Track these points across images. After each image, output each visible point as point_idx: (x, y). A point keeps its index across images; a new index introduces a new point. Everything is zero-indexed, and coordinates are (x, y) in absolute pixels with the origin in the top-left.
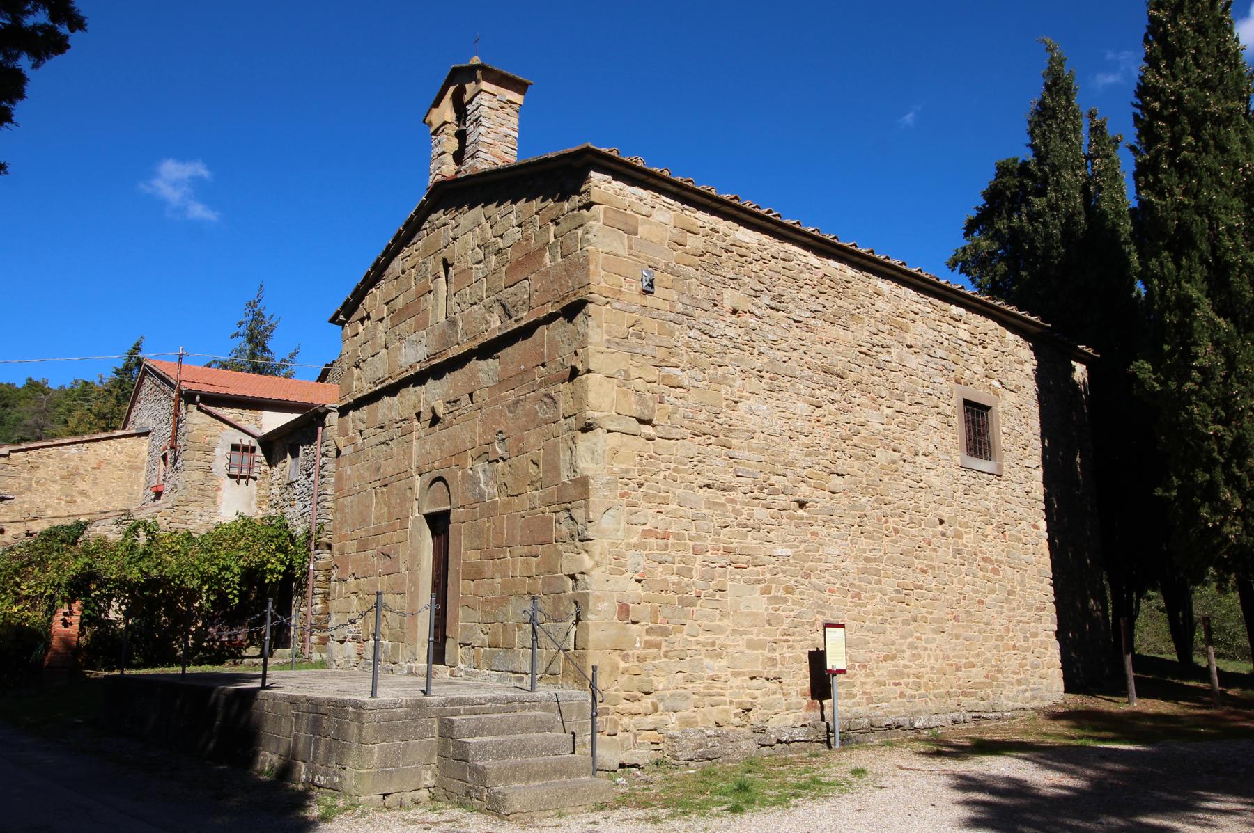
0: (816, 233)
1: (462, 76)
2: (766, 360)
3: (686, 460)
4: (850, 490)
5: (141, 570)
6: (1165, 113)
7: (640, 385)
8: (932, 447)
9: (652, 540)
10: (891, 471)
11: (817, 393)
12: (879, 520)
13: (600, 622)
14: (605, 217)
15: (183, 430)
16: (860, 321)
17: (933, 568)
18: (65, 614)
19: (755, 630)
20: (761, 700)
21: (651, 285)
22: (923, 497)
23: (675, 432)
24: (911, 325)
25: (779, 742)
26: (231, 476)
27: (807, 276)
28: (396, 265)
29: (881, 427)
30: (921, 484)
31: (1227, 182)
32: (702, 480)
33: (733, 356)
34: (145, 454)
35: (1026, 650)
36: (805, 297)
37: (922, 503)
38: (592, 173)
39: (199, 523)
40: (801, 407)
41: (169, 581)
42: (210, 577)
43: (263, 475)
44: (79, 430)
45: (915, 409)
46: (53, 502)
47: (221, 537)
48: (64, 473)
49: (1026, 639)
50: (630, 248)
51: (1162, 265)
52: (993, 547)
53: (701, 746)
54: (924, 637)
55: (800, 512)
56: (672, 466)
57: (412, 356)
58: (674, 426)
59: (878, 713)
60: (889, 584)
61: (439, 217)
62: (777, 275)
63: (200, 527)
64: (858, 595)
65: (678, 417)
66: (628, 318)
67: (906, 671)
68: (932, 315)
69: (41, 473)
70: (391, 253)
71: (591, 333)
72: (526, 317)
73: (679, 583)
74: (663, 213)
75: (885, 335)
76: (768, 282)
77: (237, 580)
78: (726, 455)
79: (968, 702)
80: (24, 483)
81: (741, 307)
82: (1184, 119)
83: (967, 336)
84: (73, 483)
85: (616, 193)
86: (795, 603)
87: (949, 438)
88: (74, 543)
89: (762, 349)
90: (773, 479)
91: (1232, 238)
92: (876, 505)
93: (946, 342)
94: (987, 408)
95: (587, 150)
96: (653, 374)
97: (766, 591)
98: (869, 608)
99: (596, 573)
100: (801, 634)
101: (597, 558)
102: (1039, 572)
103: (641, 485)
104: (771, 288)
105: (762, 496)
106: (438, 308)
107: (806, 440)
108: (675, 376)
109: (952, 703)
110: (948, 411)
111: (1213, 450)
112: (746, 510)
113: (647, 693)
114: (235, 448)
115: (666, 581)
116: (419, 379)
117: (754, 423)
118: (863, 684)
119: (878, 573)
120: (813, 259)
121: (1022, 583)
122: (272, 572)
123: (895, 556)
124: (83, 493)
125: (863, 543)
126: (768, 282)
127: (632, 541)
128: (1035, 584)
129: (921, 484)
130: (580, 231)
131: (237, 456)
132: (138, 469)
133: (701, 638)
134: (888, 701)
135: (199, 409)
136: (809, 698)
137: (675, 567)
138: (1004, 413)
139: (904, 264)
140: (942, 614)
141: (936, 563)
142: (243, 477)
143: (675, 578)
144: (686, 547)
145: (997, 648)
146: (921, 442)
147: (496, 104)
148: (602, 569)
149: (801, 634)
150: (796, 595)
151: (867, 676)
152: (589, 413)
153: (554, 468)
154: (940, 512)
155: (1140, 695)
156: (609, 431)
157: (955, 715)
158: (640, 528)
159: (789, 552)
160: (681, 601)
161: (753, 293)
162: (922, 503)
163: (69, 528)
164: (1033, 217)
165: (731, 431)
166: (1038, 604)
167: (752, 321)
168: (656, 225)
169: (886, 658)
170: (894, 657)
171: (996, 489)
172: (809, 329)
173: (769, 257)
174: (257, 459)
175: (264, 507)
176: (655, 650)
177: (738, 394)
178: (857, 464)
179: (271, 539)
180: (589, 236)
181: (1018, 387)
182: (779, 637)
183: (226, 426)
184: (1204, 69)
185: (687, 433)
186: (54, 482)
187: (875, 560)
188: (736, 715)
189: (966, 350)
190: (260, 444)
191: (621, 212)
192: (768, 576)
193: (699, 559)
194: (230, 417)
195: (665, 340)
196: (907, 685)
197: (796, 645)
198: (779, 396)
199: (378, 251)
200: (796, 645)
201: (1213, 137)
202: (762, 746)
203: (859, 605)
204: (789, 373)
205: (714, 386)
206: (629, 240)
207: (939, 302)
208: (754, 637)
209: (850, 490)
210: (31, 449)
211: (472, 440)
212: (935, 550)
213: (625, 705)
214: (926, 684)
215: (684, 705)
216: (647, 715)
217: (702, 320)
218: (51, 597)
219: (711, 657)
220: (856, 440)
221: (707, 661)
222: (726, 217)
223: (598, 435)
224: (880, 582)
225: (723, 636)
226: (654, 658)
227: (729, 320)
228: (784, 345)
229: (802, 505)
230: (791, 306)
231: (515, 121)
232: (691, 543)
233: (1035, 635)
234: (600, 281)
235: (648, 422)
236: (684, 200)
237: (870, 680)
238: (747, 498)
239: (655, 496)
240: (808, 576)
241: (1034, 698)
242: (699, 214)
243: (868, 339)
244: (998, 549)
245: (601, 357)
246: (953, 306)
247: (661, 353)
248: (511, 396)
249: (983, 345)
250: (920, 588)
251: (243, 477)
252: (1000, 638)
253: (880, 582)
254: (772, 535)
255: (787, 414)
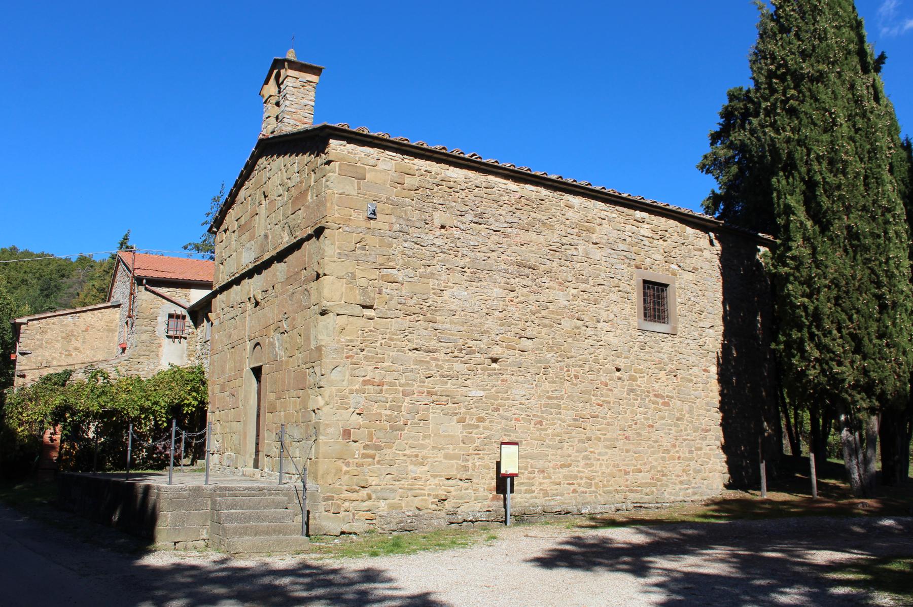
0: (512, 168)
1: (278, 64)
2: (468, 260)
3: (398, 332)
4: (537, 349)
5: (99, 404)
6: (779, 73)
7: (363, 282)
8: (612, 316)
9: (370, 387)
10: (574, 334)
11: (512, 281)
12: (562, 369)
13: (329, 440)
14: (340, 169)
15: (136, 304)
16: (551, 227)
17: (608, 402)
18: (51, 434)
19: (451, 447)
20: (453, 493)
21: (374, 213)
22: (602, 353)
23: (389, 314)
24: (598, 228)
25: (465, 521)
26: (169, 337)
27: (506, 198)
28: (242, 193)
29: (567, 303)
30: (601, 343)
31: (818, 122)
32: (411, 345)
33: (440, 258)
34: (118, 320)
35: (691, 460)
36: (504, 213)
37: (601, 357)
38: (331, 141)
39: (146, 371)
40: (497, 292)
41: (120, 412)
42: (147, 409)
43: (191, 336)
44: (87, 301)
45: (600, 289)
46: (57, 355)
47: (158, 382)
48: (64, 335)
49: (690, 452)
50: (359, 189)
51: (778, 181)
52: (665, 385)
53: (401, 522)
54: (597, 451)
55: (494, 365)
56: (387, 336)
57: (247, 260)
58: (389, 309)
59: (552, 503)
60: (568, 415)
61: (263, 161)
62: (480, 199)
63: (148, 373)
64: (541, 423)
65: (393, 303)
66: (355, 237)
67: (579, 475)
68: (618, 219)
69: (49, 336)
70: (239, 185)
71: (326, 249)
72: (300, 235)
73: (391, 415)
74: (387, 162)
75: (574, 237)
76: (472, 204)
77: (163, 411)
78: (432, 327)
79: (632, 496)
80: (38, 343)
81: (448, 224)
82: (789, 78)
83: (649, 233)
84: (70, 342)
85: (348, 152)
86: (485, 428)
87: (628, 309)
88: (64, 385)
89: (465, 253)
90: (470, 343)
91: (820, 164)
92: (559, 359)
93: (629, 239)
94: (666, 286)
95: (325, 127)
96: (375, 274)
97: (461, 421)
98: (549, 431)
99: (326, 409)
100: (489, 449)
101: (327, 399)
102: (707, 404)
103: (362, 350)
104: (475, 208)
105: (461, 355)
106: (261, 225)
107: (500, 315)
108: (392, 275)
109: (619, 497)
110: (629, 289)
111: (802, 316)
112: (446, 365)
113: (363, 487)
114: (171, 316)
115: (380, 414)
116: (249, 274)
117: (456, 305)
118: (541, 484)
119: (559, 407)
120: (511, 185)
121: (690, 411)
122: (189, 405)
123: (574, 394)
124: (76, 349)
125: (547, 385)
126: (472, 204)
127: (354, 388)
128: (702, 412)
129: (601, 343)
130: (324, 180)
131: (173, 322)
132: (112, 331)
133: (407, 452)
134: (562, 495)
135: (146, 289)
136: (495, 493)
137: (387, 405)
138: (681, 288)
139: (589, 184)
140: (615, 435)
141: (611, 399)
142: (177, 337)
143: (388, 412)
144: (396, 392)
145: (663, 459)
146: (602, 312)
147: (298, 84)
148: (331, 406)
149: (489, 449)
150: (487, 423)
151: (544, 478)
152: (324, 303)
153: (308, 339)
154: (617, 363)
155: (768, 490)
156: (338, 315)
157: (619, 506)
158: (361, 379)
159: (482, 393)
160: (391, 427)
161: (459, 213)
162: (601, 357)
163: (60, 374)
164: (753, 132)
165: (436, 311)
166: (704, 427)
167: (457, 233)
168: (381, 171)
169: (562, 466)
170: (570, 465)
171: (670, 344)
172: (506, 236)
173: (473, 187)
174: (187, 324)
175: (192, 359)
176: (370, 460)
177: (443, 285)
178: (544, 330)
179: (188, 382)
180: (328, 183)
181: (696, 269)
182: (471, 451)
183: (165, 301)
184: (803, 41)
185: (401, 314)
186: (57, 341)
187: (557, 398)
188: (432, 503)
189: (647, 243)
190: (189, 313)
191: (353, 165)
192: (463, 410)
193: (407, 399)
194: (167, 295)
195: (385, 250)
196: (579, 485)
197: (486, 457)
198: (479, 284)
199: (230, 186)
200: (486, 457)
201: (810, 90)
202: (451, 523)
203: (541, 429)
204: (487, 268)
205: (425, 280)
206: (359, 184)
207: (625, 210)
208: (450, 451)
209: (537, 349)
210: (45, 318)
211: (273, 319)
212: (611, 390)
213: (346, 495)
214: (596, 484)
215: (392, 495)
216: (363, 501)
217: (415, 235)
218: (42, 422)
219: (415, 465)
220: (544, 313)
221: (411, 467)
222: (439, 161)
223: (330, 318)
224: (560, 413)
225: (425, 451)
226: (369, 465)
227: (437, 233)
228: (484, 249)
229: (495, 360)
230: (491, 220)
231: (312, 94)
232: (401, 389)
233: (700, 449)
234: (334, 214)
235: (371, 307)
236: (403, 152)
237: (548, 481)
238: (448, 357)
239: (373, 357)
240: (498, 410)
241: (695, 494)
242: (417, 161)
243: (558, 240)
244: (670, 388)
245: (334, 265)
246: (637, 212)
247: (380, 260)
248: (291, 289)
249: (663, 238)
250: (597, 417)
251: (177, 337)
252: (668, 451)
253: (560, 413)
254: (468, 382)
255: (485, 297)
